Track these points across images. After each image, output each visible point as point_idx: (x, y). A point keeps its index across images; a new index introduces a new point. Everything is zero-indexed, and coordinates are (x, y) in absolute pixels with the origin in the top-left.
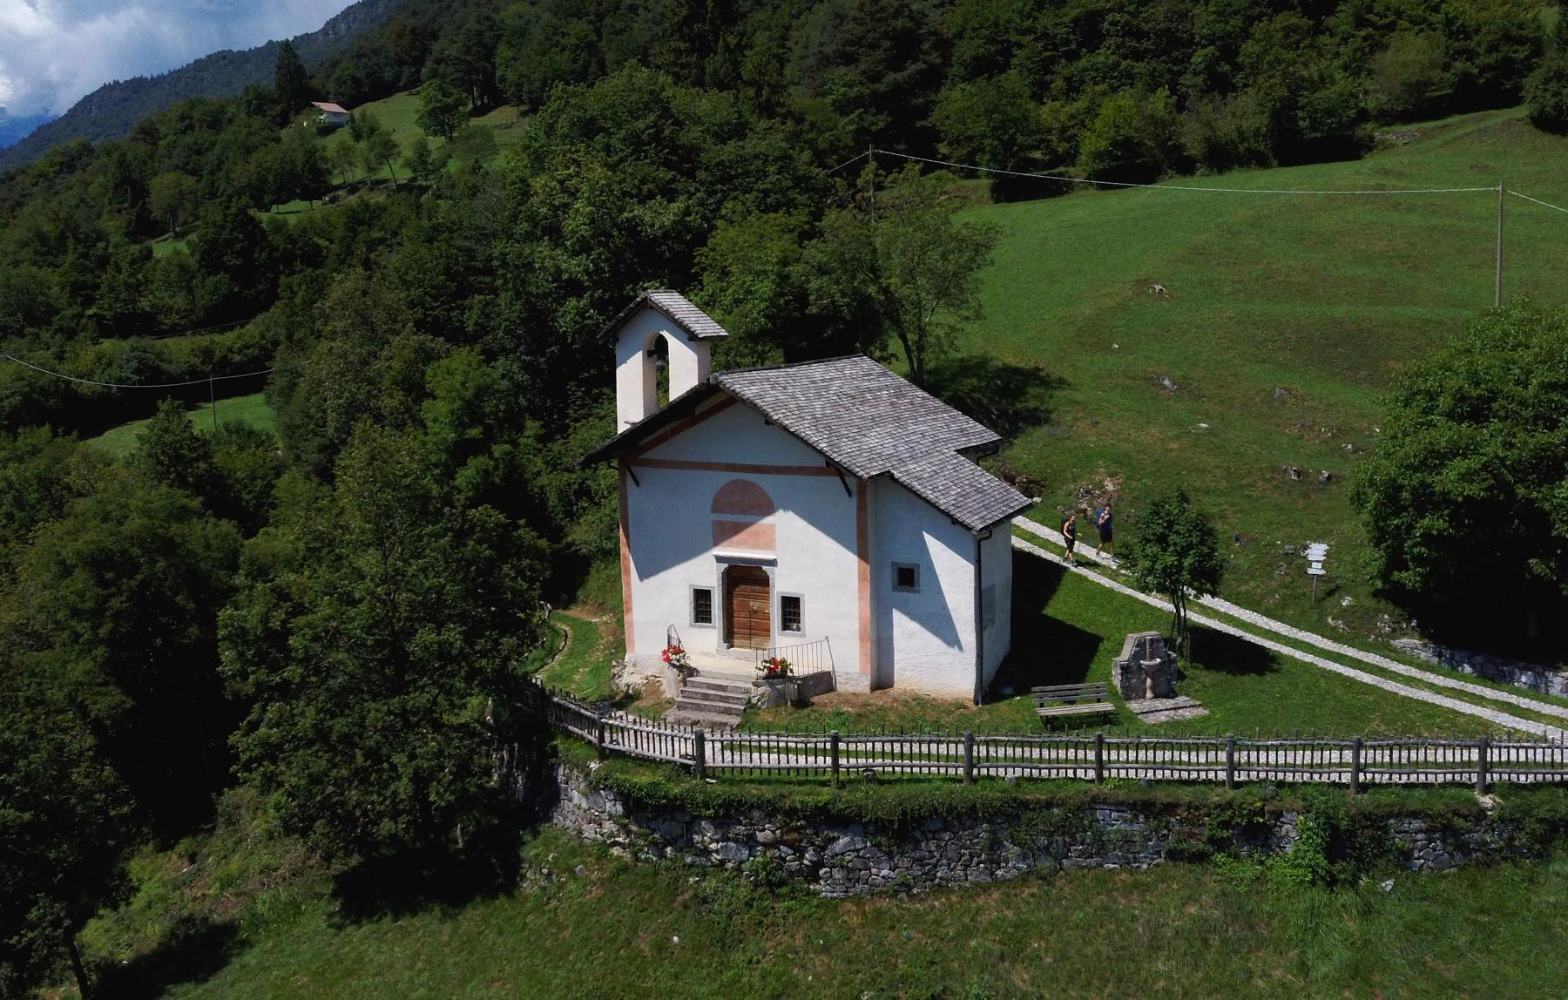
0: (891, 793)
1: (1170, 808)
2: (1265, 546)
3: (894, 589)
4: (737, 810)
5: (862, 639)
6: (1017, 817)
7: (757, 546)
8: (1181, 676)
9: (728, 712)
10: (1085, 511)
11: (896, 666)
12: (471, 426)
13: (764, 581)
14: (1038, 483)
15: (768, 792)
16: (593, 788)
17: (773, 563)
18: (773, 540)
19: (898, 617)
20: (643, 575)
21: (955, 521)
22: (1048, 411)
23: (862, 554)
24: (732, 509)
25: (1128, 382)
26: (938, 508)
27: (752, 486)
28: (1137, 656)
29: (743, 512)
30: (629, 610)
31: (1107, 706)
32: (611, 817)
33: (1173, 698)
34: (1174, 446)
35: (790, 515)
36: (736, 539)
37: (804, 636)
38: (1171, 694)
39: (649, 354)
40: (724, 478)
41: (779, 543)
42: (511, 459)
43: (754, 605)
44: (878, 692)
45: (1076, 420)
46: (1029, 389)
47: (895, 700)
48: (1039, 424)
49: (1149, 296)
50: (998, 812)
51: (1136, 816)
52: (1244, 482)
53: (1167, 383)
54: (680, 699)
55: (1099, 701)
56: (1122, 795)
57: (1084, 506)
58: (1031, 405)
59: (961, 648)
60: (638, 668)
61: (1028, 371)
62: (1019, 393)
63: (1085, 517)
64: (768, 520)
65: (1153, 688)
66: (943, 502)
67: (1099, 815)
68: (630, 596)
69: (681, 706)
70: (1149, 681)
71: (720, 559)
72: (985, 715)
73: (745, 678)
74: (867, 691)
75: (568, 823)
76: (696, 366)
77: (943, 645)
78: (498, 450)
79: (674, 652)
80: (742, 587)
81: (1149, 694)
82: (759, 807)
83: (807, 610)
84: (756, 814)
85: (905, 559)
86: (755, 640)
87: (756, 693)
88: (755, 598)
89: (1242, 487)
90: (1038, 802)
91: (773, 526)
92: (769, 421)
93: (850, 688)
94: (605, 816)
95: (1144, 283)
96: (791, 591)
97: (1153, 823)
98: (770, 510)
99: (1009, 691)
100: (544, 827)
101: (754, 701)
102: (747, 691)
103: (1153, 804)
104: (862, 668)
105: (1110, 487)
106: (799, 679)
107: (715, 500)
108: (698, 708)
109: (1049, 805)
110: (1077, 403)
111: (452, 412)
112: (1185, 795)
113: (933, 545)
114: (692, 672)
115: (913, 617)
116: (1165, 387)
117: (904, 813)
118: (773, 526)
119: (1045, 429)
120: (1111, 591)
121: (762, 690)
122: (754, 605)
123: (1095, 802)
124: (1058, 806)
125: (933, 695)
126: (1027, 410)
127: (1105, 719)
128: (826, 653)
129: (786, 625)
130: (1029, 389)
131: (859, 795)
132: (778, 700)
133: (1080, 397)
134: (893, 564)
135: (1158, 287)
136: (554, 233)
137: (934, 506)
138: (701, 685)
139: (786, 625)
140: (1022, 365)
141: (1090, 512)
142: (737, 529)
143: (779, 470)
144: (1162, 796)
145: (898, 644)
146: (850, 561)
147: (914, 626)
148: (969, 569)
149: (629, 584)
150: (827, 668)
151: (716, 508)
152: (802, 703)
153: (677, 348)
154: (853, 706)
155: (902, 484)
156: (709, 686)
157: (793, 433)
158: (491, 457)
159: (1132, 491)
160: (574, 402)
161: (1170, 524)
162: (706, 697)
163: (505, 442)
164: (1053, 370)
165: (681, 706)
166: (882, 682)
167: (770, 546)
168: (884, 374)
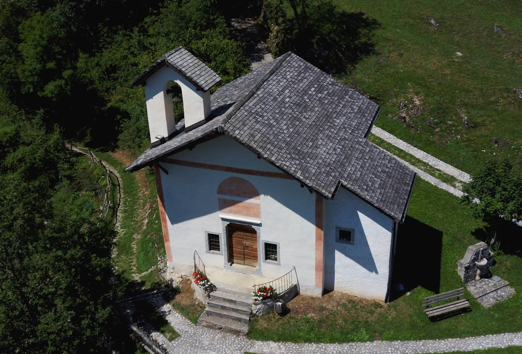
2: (514, 149)
3: (336, 241)
5: (317, 269)
7: (248, 215)
8: (494, 263)
9: (239, 320)
10: (404, 118)
11: (335, 281)
12: (49, 60)
17: (260, 225)
18: (260, 212)
19: (339, 256)
20: (173, 222)
21: (382, 211)
22: (373, 45)
23: (319, 224)
25: (411, 21)
26: (372, 205)
27: (245, 181)
30: (168, 240)
31: (464, 304)
34: (448, 71)
37: (279, 264)
39: (168, 92)
41: (262, 214)
43: (247, 243)
45: (390, 52)
47: (338, 304)
52: (492, 99)
53: (433, 22)
54: (207, 309)
55: (458, 299)
57: (404, 115)
58: (363, 40)
59: (377, 272)
61: (356, 14)
62: (356, 35)
63: (405, 121)
68: (167, 233)
69: (209, 313)
70: (478, 272)
71: (223, 219)
73: (248, 296)
76: (202, 105)
78: (66, 73)
79: (201, 277)
80: (239, 233)
81: (478, 278)
83: (281, 251)
85: (345, 225)
87: (255, 309)
88: (246, 239)
89: (492, 103)
91: (259, 205)
93: (309, 293)
96: (271, 240)
98: (255, 194)
99: (401, 287)
101: (254, 312)
102: (249, 305)
105: (418, 103)
107: (220, 187)
108: (220, 315)
110: (389, 40)
111: (37, 53)
113: (362, 217)
114: (212, 288)
118: (259, 205)
119: (372, 60)
120: (435, 188)
122: (247, 243)
127: (464, 310)
129: (267, 257)
134: (337, 228)
138: (219, 298)
139: (267, 257)
140: (353, 11)
141: (407, 119)
142: (233, 203)
143: (262, 174)
145: (337, 264)
146: (310, 229)
149: (166, 227)
153: (186, 91)
154: (314, 311)
155: (348, 189)
156: (224, 300)
158: (63, 78)
159: (430, 104)
160: (103, 35)
161: (498, 183)
162: (223, 308)
163: (69, 68)
164: (370, 14)
165: (209, 313)
166: (328, 289)
168: (306, 69)
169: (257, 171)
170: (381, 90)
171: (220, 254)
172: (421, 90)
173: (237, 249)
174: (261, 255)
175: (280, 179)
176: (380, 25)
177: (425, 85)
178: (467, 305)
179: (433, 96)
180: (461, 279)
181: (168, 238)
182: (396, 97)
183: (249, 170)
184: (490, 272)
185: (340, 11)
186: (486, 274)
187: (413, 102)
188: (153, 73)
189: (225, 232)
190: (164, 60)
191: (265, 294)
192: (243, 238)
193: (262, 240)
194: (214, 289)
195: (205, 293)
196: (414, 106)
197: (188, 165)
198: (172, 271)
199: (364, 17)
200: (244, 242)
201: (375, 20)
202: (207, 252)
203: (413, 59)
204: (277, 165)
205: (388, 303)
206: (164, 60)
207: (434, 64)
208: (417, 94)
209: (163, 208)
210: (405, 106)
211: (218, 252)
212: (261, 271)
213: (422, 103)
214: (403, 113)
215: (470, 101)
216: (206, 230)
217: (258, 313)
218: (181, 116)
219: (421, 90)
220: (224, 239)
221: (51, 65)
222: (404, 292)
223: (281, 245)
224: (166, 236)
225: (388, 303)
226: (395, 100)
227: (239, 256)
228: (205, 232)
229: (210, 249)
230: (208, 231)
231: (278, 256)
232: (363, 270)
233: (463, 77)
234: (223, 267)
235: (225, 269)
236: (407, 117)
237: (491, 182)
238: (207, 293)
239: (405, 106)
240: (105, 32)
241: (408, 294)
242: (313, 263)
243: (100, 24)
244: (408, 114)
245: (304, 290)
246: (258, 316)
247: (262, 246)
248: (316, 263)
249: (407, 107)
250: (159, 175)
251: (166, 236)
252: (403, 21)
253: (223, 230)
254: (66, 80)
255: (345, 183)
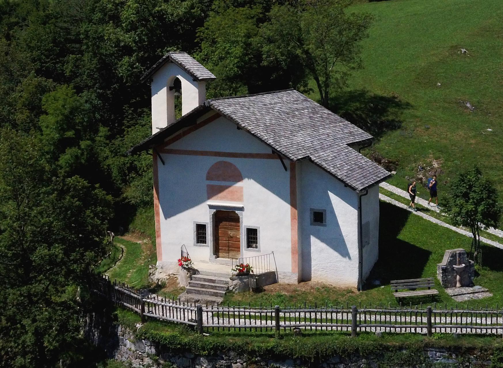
0: (310, 342)
1: (471, 350)
3: (311, 224)
4: (221, 351)
5: (293, 253)
6: (382, 355)
7: (233, 200)
8: (477, 274)
9: (216, 295)
10: (421, 179)
11: (313, 269)
12: (68, 130)
13: (236, 220)
14: (394, 163)
15: (239, 341)
16: (139, 338)
17: (242, 209)
18: (242, 196)
19: (313, 240)
20: (167, 216)
21: (346, 185)
23: (293, 204)
24: (218, 178)
25: (446, 105)
26: (336, 178)
28: (451, 263)
29: (224, 180)
30: (159, 236)
31: (434, 292)
32: (148, 355)
33: (472, 287)
34: (473, 141)
35: (252, 181)
36: (220, 195)
37: (259, 251)
38: (471, 284)
39: (170, 89)
40: (214, 160)
41: (245, 197)
42: (91, 149)
43: (231, 233)
44: (302, 283)
45: (416, 126)
46: (389, 109)
47: (312, 288)
48: (395, 129)
49: (458, 55)
50: (371, 353)
51: (451, 355)
53: (468, 105)
54: (188, 287)
55: (429, 288)
56: (442, 343)
57: (421, 176)
58: (390, 118)
59: (350, 258)
60: (164, 270)
63: (422, 183)
64: (239, 184)
65: (460, 281)
66: (339, 174)
67: (429, 354)
69: (189, 292)
71: (211, 207)
72: (363, 296)
74: (296, 282)
75: (124, 359)
76: (197, 95)
77: (340, 256)
78: (83, 144)
81: (458, 285)
82: (234, 350)
83: (262, 237)
84: (232, 354)
85: (318, 206)
86: (231, 254)
90: (395, 347)
91: (241, 188)
92: (239, 127)
94: (145, 355)
95: (456, 47)
96: (252, 225)
97: (461, 359)
98: (239, 178)
99: (377, 282)
100: (110, 361)
101: (231, 288)
103: (461, 348)
104: (293, 270)
105: (436, 165)
106: (257, 276)
108: (199, 292)
109: (401, 348)
111: (57, 122)
112: (479, 343)
115: (322, 240)
116: (467, 108)
117: (317, 353)
118: (241, 188)
119: (398, 132)
121: (235, 282)
122: (231, 233)
123: (427, 346)
124: (406, 349)
125: (334, 285)
126: (388, 121)
127: (433, 299)
128: (272, 261)
129: (249, 245)
130: (389, 109)
131: (291, 343)
132: (245, 288)
133: (419, 114)
134: (311, 209)
135: (463, 50)
136: (116, 19)
137: (334, 176)
138: (200, 279)
139: (249, 245)
140: (385, 95)
144: (466, 343)
145: (313, 249)
147: (323, 245)
148: (355, 212)
150: (273, 270)
151: (209, 178)
152: (258, 289)
153: (186, 85)
155: (316, 164)
157: (253, 134)
158: (79, 148)
162: (203, 286)
163: (88, 139)
164: (403, 98)
165: (189, 292)
167: (240, 199)
168: (306, 100)
169: (241, 154)
170: (401, 156)
171: (206, 246)
172: (441, 156)
173: (222, 241)
175: (260, 159)
176: (412, 106)
177: (447, 152)
178: (435, 293)
179: (453, 161)
180: (440, 283)
181: (160, 233)
182: (415, 162)
184: (472, 283)
185: (372, 94)
186: (467, 283)
187: (432, 165)
188: (159, 68)
190: (169, 56)
191: (241, 269)
192: (228, 228)
194: (197, 273)
195: (187, 274)
196: (432, 169)
197: (183, 154)
198: (160, 271)
199: (396, 100)
200: (229, 232)
201: (409, 103)
202: (194, 245)
203: (439, 132)
204: (252, 132)
205: (361, 291)
206: (169, 56)
207: (460, 136)
208: (437, 159)
209: (158, 200)
210: (422, 168)
211: (204, 244)
213: (441, 165)
214: (419, 175)
215: (490, 164)
216: (194, 221)
217: (234, 290)
219: (441, 156)
221: (70, 134)
222: (380, 286)
224: (157, 232)
225: (361, 291)
226: (414, 165)
228: (194, 222)
229: (198, 243)
230: (196, 221)
231: (258, 245)
232: (335, 255)
233: (487, 146)
236: (424, 178)
237: (463, 187)
238: (189, 274)
239: (422, 168)
240: (130, 114)
241: (383, 287)
242: (289, 245)
243: (125, 106)
244: (424, 175)
245: (282, 277)
246: (234, 293)
248: (292, 245)
249: (425, 169)
250: (157, 162)
251: (157, 232)
252: (438, 104)
254: (83, 150)
255: (313, 158)
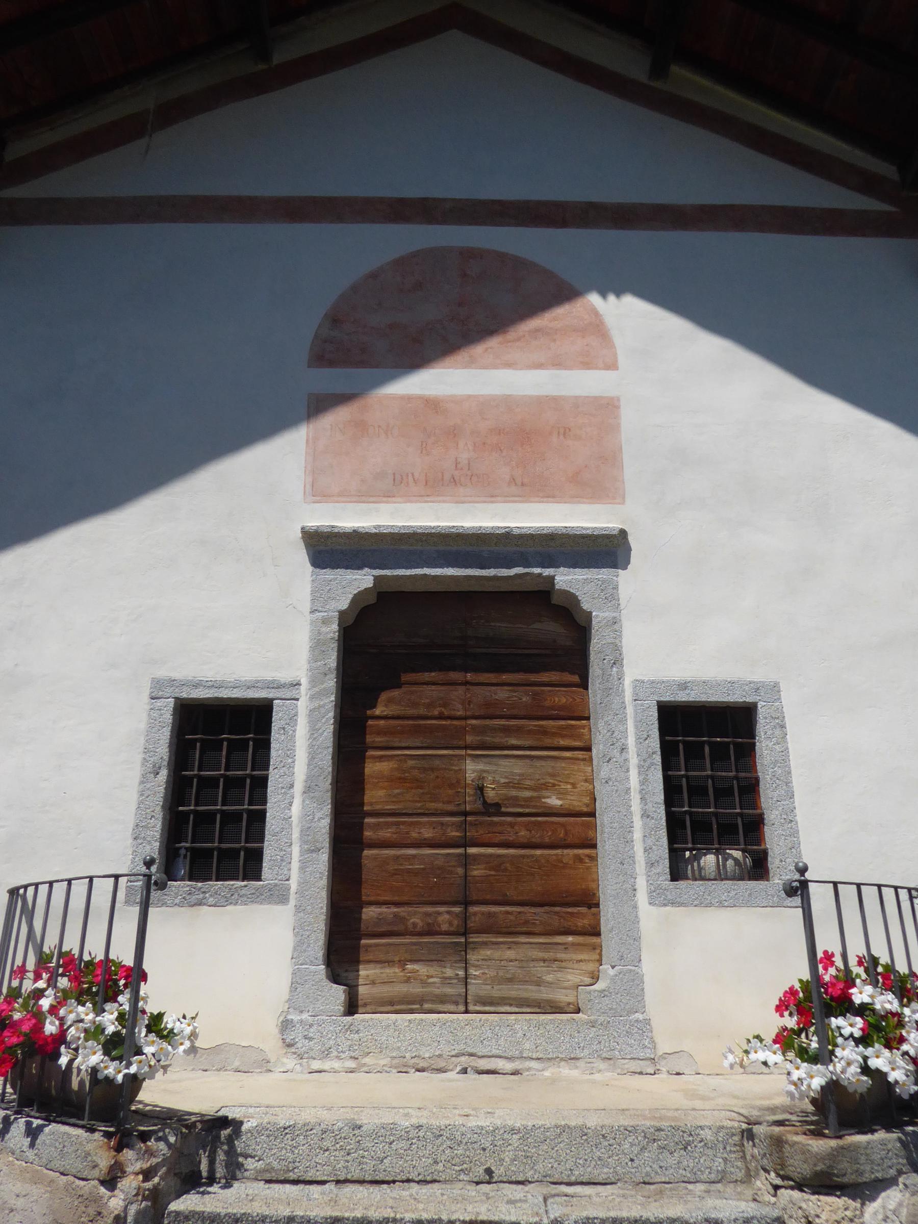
107: (334, 319)
162: (506, 730)
174: (638, 823)
183: (539, 203)
189: (332, 660)
193: (638, 683)
200: (472, 769)
212: (640, 1006)
218: (90, 881)
220: (313, 730)
223: (790, 701)
227: (416, 917)
234: (271, 1044)
235: (290, 1062)
247: (641, 740)
253: (317, 645)
